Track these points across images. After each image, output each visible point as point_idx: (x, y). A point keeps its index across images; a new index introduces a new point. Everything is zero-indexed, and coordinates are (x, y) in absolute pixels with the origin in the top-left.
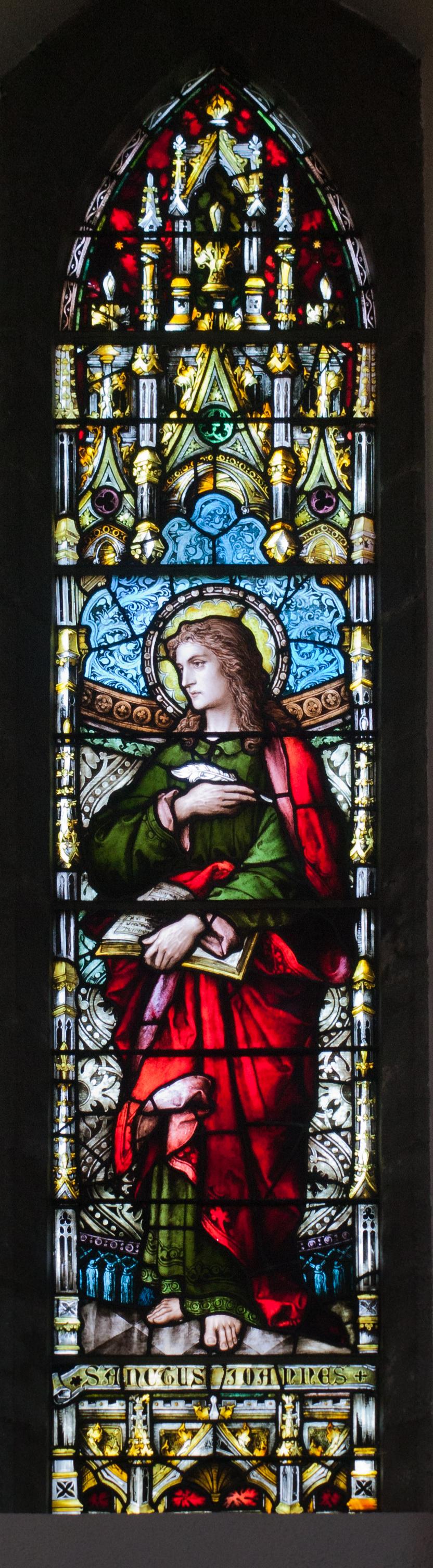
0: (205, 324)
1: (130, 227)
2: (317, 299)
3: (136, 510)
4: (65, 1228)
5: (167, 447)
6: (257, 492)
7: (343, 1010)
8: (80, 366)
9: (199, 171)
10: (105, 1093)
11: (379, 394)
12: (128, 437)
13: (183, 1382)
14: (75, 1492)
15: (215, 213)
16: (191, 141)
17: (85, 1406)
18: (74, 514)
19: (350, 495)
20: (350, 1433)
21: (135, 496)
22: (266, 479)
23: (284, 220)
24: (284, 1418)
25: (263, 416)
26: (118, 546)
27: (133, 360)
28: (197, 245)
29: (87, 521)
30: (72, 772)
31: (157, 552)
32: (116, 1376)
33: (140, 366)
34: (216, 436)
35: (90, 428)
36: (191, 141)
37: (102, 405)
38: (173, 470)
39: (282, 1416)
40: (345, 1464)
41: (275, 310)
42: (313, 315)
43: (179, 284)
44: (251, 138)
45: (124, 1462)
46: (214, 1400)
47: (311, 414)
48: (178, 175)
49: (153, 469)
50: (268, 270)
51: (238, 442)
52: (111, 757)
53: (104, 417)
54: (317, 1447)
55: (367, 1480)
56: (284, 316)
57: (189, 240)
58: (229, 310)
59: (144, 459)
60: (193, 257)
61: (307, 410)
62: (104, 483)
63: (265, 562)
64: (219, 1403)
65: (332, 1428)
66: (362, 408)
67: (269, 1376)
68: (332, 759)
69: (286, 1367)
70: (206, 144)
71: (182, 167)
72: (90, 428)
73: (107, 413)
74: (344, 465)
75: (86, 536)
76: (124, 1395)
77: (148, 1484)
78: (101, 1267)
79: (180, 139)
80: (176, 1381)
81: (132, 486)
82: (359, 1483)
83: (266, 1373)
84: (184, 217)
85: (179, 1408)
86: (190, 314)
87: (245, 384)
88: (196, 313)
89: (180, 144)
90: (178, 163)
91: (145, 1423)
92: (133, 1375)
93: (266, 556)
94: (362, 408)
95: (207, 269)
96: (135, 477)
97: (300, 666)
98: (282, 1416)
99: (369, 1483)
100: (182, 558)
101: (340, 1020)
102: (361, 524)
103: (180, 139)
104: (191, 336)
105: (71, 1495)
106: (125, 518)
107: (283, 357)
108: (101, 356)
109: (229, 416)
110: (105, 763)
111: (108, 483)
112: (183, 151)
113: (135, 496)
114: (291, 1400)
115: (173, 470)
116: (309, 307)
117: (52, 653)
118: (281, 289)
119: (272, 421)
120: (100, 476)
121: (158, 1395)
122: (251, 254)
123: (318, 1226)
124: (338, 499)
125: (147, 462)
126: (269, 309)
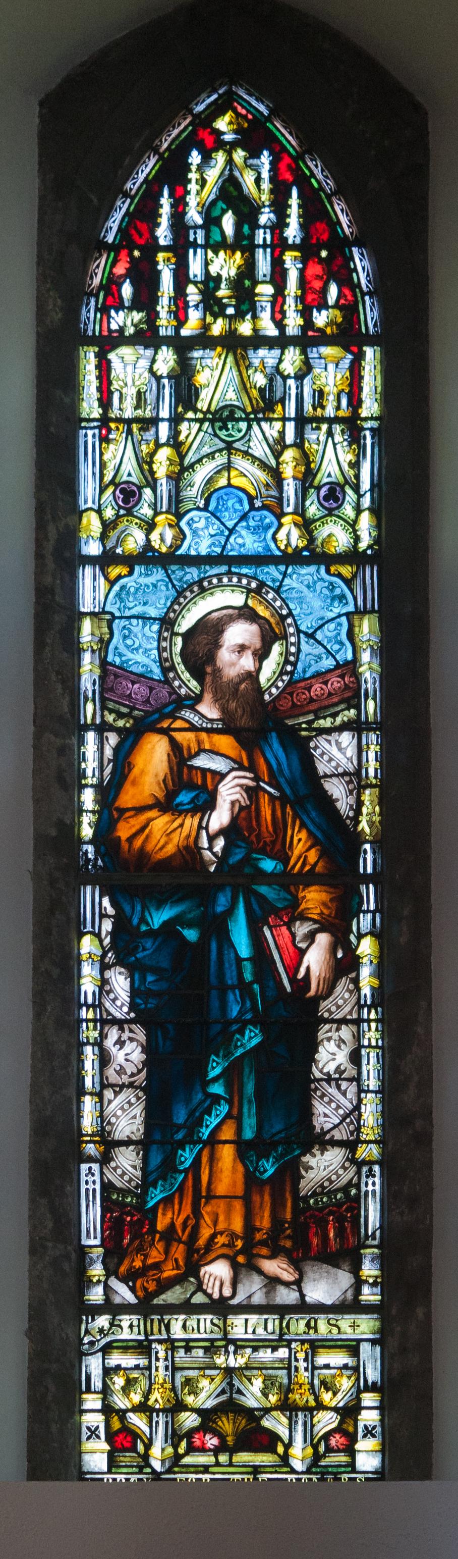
0: (218, 328)
2: (323, 305)
3: (155, 504)
4: (91, 1183)
5: (184, 443)
8: (104, 368)
9: (214, 182)
10: (128, 1057)
11: (388, 395)
12: (150, 435)
13: (202, 1330)
14: (103, 1435)
15: (228, 223)
19: (356, 488)
20: (358, 1379)
21: (154, 491)
23: (293, 232)
27: (281, 361)
28: (210, 254)
29: (109, 513)
31: (176, 540)
34: (233, 433)
35: (113, 425)
38: (192, 466)
40: (350, 1411)
41: (283, 313)
42: (321, 319)
44: (262, 153)
46: (231, 1348)
48: (193, 187)
50: (278, 277)
53: (126, 417)
55: (96, 1424)
56: (293, 323)
58: (240, 315)
59: (164, 454)
62: (125, 478)
64: (235, 1353)
65: (341, 1375)
67: (139, 1326)
68: (340, 741)
69: (152, 1317)
71: (197, 180)
72: (113, 425)
73: (128, 414)
74: (350, 461)
75: (107, 526)
76: (281, 1341)
77: (309, 1428)
79: (195, 153)
80: (196, 1331)
82: (365, 1426)
83: (135, 1323)
86: (204, 319)
87: (258, 386)
88: (209, 319)
89: (195, 158)
90: (193, 176)
91: (167, 1368)
95: (219, 276)
96: (282, 473)
99: (374, 1427)
100: (204, 552)
103: (195, 153)
104: (204, 340)
106: (146, 511)
107: (168, 360)
112: (198, 165)
113: (154, 491)
114: (164, 1349)
115: (192, 466)
117: (76, 640)
118: (289, 295)
119: (284, 419)
120: (121, 472)
121: (320, 1344)
122: (263, 263)
124: (344, 493)
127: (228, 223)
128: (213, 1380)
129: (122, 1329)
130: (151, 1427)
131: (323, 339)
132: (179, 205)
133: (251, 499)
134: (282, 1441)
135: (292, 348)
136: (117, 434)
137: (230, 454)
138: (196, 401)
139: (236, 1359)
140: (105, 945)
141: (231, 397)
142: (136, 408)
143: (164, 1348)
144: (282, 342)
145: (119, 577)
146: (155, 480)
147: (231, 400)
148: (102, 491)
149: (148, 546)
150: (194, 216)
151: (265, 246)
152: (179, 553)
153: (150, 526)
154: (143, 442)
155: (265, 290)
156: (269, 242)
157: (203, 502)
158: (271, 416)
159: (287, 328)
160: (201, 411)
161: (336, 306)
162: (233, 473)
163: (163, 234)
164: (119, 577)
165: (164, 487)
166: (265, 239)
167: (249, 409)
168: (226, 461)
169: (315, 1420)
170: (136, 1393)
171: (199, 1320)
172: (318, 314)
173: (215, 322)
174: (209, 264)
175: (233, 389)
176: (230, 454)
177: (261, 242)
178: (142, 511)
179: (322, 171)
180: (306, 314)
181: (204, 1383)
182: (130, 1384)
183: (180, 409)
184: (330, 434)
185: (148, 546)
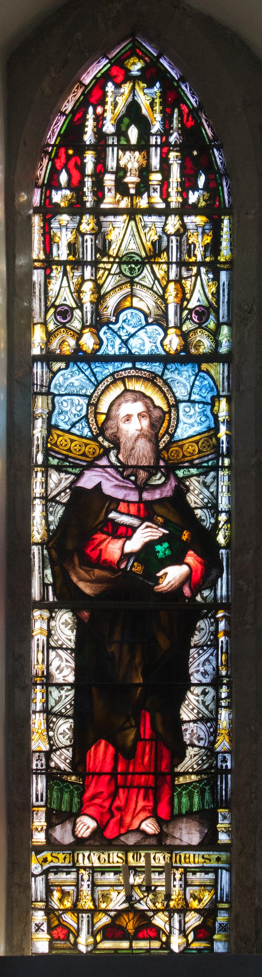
1: (102, 219)
2: (195, 188)
6: (158, 307)
7: (212, 634)
13: (111, 860)
15: (133, 134)
16: (118, 86)
17: (51, 876)
18: (45, 324)
22: (163, 298)
24: (175, 884)
25: (163, 261)
26: (72, 342)
28: (120, 153)
30: (35, 481)
32: (70, 858)
33: (84, 228)
36: (118, 86)
37: (60, 252)
39: (173, 882)
41: (168, 195)
42: (193, 197)
43: (109, 180)
45: (75, 909)
47: (193, 259)
48: (109, 107)
49: (93, 293)
51: (146, 276)
52: (67, 476)
54: (194, 900)
56: (175, 200)
57: (116, 149)
58: (139, 194)
59: (88, 287)
60: (118, 160)
61: (190, 257)
63: (163, 353)
66: (225, 253)
70: (126, 88)
73: (64, 257)
78: (61, 791)
79: (110, 84)
81: (80, 306)
84: (113, 135)
85: (110, 877)
89: (110, 87)
92: (81, 856)
93: (164, 350)
94: (225, 253)
97: (186, 423)
98: (173, 882)
101: (210, 640)
102: (225, 330)
103: (110, 84)
105: (43, 931)
106: (76, 325)
108: (59, 221)
109: (140, 260)
110: (64, 480)
111: (65, 303)
116: (191, 193)
119: (169, 263)
122: (155, 162)
123: (195, 766)
125: (89, 290)
126: (165, 196)
127: (133, 134)
128: (119, 893)
129: (58, 859)
130: (78, 924)
131: (194, 210)
132: (99, 119)
133: (146, 316)
134: (164, 932)
135: (173, 216)
136: (57, 273)
137: (132, 285)
138: (109, 249)
139: (135, 880)
140: (62, 750)
141: (133, 247)
142: (68, 255)
143: (87, 873)
144: (166, 212)
145: (60, 370)
146: (82, 305)
147: (132, 249)
148: (47, 311)
149: (78, 348)
150: (109, 128)
151: (156, 146)
152: (98, 353)
153: (79, 336)
154: (74, 277)
155: (156, 178)
156: (159, 143)
157: (114, 318)
158: (160, 260)
159: (171, 203)
160: (112, 256)
161: (204, 189)
162: (135, 299)
163: (89, 138)
164: (60, 370)
165: (88, 307)
166: (156, 142)
167: (144, 254)
168: (129, 290)
169: (187, 919)
170: (68, 902)
171: (109, 855)
172: (192, 194)
173: (123, 199)
174: (120, 160)
175: (134, 241)
176: (132, 285)
177: (154, 143)
178: (73, 325)
179: (190, 90)
180: (183, 193)
181: (114, 895)
182: (64, 894)
183: (98, 255)
184: (198, 273)
185: (78, 348)
